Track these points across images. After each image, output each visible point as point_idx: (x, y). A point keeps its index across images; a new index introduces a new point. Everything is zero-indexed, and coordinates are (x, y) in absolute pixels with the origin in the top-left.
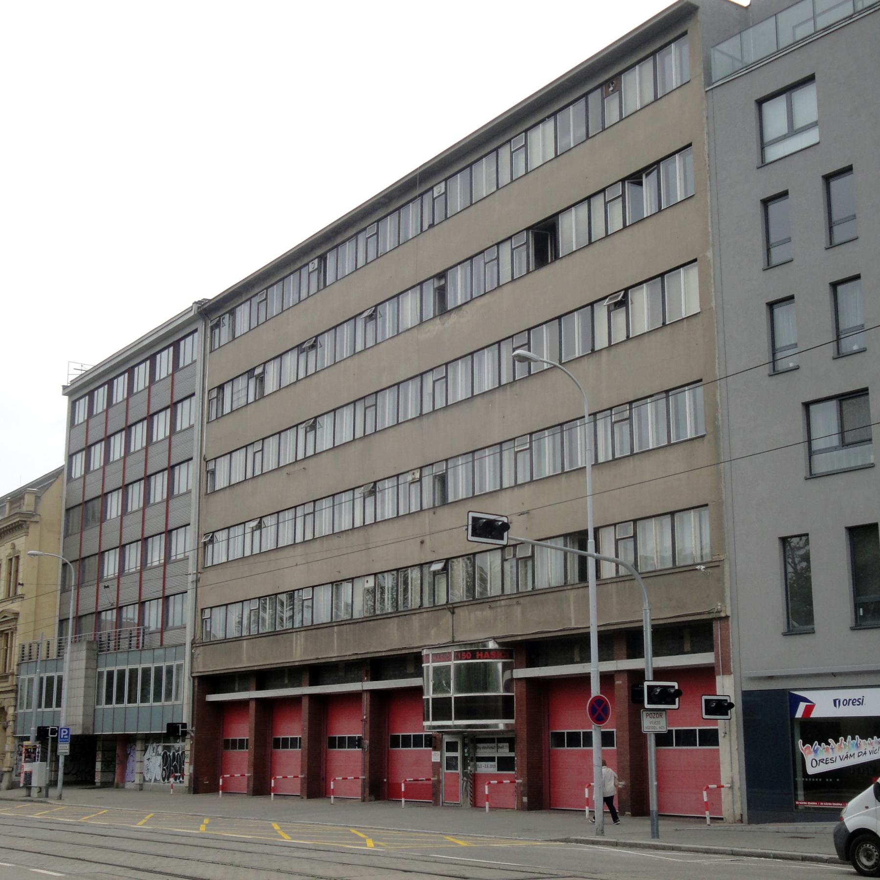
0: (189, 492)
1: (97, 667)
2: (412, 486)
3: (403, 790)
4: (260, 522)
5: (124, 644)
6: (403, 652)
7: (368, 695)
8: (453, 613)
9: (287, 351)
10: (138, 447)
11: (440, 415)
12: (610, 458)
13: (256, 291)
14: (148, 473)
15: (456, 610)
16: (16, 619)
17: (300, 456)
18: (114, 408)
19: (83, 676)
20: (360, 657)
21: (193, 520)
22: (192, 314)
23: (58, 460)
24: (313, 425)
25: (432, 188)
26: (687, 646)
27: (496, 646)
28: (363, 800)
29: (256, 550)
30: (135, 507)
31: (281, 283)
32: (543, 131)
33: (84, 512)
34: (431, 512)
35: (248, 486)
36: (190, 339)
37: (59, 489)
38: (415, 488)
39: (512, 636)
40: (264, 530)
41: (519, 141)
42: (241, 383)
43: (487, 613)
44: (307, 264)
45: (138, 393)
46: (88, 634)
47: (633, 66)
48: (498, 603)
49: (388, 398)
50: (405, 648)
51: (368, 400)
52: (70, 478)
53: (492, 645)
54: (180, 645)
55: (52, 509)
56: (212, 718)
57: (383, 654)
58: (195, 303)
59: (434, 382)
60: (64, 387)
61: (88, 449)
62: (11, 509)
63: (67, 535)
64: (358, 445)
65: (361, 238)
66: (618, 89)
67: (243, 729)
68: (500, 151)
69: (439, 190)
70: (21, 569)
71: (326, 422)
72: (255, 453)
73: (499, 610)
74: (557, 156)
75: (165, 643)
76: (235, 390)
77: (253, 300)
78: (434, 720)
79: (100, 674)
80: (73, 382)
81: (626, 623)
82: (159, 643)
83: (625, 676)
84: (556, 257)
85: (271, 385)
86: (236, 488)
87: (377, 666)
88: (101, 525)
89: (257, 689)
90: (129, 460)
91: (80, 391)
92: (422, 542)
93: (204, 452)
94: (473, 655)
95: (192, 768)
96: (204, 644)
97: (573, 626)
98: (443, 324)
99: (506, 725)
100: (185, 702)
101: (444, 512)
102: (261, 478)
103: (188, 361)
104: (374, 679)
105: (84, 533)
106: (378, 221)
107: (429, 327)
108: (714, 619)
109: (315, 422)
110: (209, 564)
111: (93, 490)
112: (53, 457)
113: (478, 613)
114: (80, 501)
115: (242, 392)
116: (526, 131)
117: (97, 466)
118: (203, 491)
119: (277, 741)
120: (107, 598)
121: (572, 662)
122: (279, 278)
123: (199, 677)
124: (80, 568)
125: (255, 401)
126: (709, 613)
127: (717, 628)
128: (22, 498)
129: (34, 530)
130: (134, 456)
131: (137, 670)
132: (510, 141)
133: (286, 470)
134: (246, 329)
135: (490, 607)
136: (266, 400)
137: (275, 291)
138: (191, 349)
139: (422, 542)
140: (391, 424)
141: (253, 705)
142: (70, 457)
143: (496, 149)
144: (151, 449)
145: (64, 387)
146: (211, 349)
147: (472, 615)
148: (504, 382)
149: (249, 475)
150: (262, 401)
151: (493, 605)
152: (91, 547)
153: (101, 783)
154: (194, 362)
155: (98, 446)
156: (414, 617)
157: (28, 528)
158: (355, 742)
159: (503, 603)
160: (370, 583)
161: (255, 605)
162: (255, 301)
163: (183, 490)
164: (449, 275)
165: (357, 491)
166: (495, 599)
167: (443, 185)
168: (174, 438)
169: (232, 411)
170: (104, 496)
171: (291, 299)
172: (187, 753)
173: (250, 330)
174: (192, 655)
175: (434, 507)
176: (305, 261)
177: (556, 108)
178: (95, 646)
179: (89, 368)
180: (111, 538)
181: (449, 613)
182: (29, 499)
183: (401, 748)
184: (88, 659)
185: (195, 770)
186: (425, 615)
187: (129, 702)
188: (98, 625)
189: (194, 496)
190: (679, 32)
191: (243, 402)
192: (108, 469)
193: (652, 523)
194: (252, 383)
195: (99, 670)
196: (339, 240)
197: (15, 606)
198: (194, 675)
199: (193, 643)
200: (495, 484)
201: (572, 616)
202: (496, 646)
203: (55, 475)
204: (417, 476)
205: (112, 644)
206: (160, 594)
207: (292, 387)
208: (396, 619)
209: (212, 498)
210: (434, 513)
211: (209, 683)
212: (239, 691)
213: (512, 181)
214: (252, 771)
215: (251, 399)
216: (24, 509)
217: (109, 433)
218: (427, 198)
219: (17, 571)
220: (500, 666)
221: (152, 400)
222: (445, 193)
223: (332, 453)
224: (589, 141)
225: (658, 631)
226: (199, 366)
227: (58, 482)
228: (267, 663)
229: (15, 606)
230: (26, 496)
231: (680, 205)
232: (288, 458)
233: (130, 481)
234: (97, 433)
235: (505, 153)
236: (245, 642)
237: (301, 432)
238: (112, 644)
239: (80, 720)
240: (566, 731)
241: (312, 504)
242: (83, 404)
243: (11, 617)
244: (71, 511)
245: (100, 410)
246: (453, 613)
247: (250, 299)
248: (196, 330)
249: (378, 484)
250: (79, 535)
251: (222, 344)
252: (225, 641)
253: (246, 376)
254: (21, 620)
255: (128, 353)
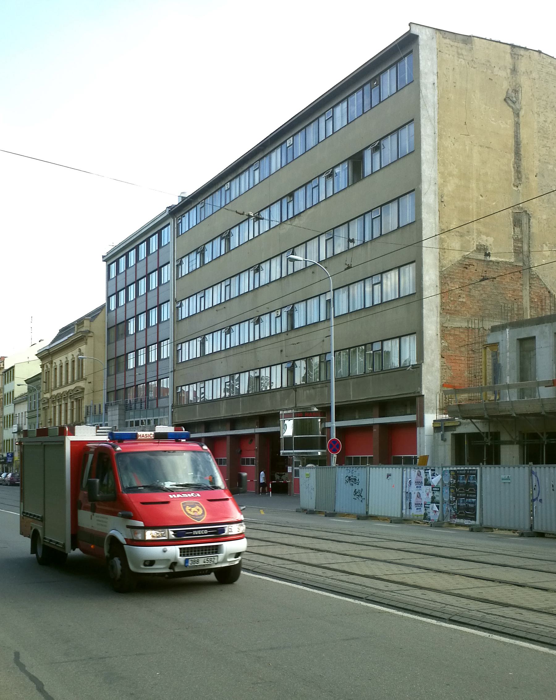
0: (168, 320)
2: (277, 319)
5: (138, 406)
6: (273, 412)
8: (296, 391)
11: (290, 277)
15: (297, 390)
16: (83, 392)
20: (252, 415)
22: (166, 214)
23: (103, 301)
24: (258, 269)
25: (286, 141)
26: (409, 411)
27: (317, 410)
31: (211, 196)
32: (342, 107)
33: (117, 330)
35: (198, 317)
37: (103, 316)
38: (278, 320)
39: (323, 404)
40: (261, 324)
41: (329, 114)
42: (217, 242)
43: (312, 391)
44: (224, 185)
46: (121, 401)
47: (386, 70)
50: (273, 410)
52: (109, 310)
54: (166, 407)
55: (99, 327)
57: (263, 413)
59: (326, 240)
60: (103, 257)
61: (117, 293)
62: (78, 329)
63: (109, 343)
64: (251, 294)
65: (252, 169)
66: (379, 84)
70: (84, 364)
72: (226, 286)
73: (317, 389)
74: (348, 123)
75: (159, 406)
76: (190, 260)
80: (108, 253)
81: (376, 398)
84: (364, 178)
86: (192, 318)
89: (205, 432)
90: (138, 300)
91: (111, 259)
92: (281, 351)
94: (303, 414)
97: (352, 399)
99: (322, 453)
101: (292, 334)
102: (203, 312)
105: (117, 342)
106: (259, 160)
107: (284, 226)
108: (416, 396)
109: (259, 267)
112: (98, 298)
113: (308, 391)
114: (115, 324)
118: (175, 320)
120: (130, 380)
122: (210, 194)
124: (117, 363)
125: (200, 267)
126: (414, 393)
127: (418, 399)
128: (83, 323)
129: (90, 341)
130: (141, 298)
132: (325, 113)
133: (216, 308)
134: (195, 224)
135: (313, 388)
136: (206, 266)
138: (167, 234)
139: (281, 351)
142: (108, 298)
144: (149, 294)
145: (103, 257)
146: (178, 234)
147: (305, 392)
149: (198, 311)
150: (229, 254)
151: (314, 386)
152: (121, 352)
154: (169, 243)
156: (277, 393)
157: (87, 340)
158: (253, 462)
159: (319, 386)
162: (199, 206)
163: (165, 319)
164: (296, 194)
165: (251, 321)
166: (316, 383)
167: (291, 139)
170: (126, 322)
172: (452, 432)
175: (288, 331)
176: (223, 183)
177: (347, 94)
178: (123, 407)
180: (130, 346)
182: (86, 323)
186: (283, 392)
189: (171, 321)
190: (409, 51)
191: (194, 268)
193: (407, 338)
194: (198, 256)
195: (126, 420)
196: (240, 171)
197: (81, 384)
200: (361, 305)
201: (351, 393)
202: (317, 410)
203: (101, 308)
204: (279, 313)
206: (144, 381)
209: (180, 324)
212: (197, 433)
213: (326, 138)
215: (198, 266)
216: (83, 329)
217: (127, 284)
218: (284, 147)
219: (82, 364)
222: (293, 144)
223: (237, 299)
226: (171, 245)
227: (103, 312)
229: (81, 384)
230: (85, 321)
231: (408, 157)
232: (275, 275)
234: (121, 285)
237: (252, 273)
241: (380, 275)
242: (113, 266)
243: (80, 390)
244: (110, 330)
246: (296, 391)
247: (196, 206)
248: (169, 224)
249: (296, 306)
250: (114, 344)
252: (213, 401)
254: (86, 392)
255: (135, 237)
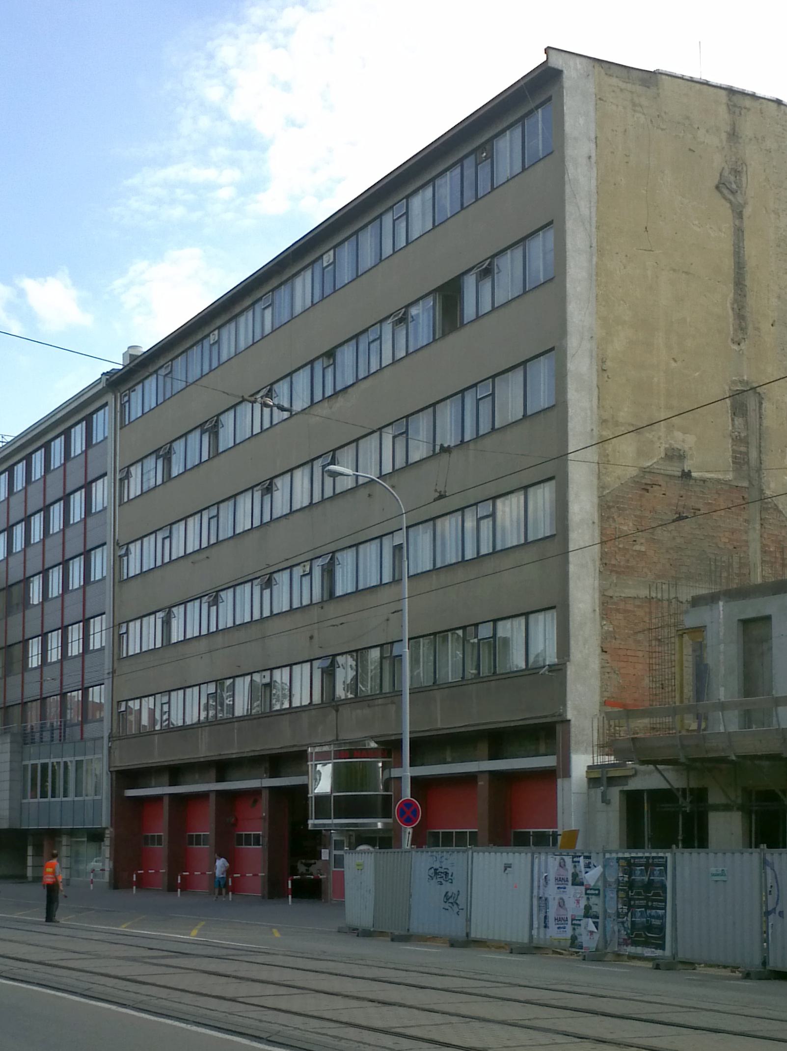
1: (22, 760)
2: (304, 579)
3: (290, 887)
4: (332, 559)
5: (47, 736)
7: (267, 791)
8: (337, 711)
9: (299, 369)
10: (77, 519)
12: (522, 541)
13: (162, 362)
14: (66, 558)
15: (340, 709)
17: (205, 544)
18: (94, 449)
19: (8, 769)
21: (109, 609)
22: (100, 387)
24: (269, 489)
28: (263, 897)
29: (213, 629)
30: (55, 594)
34: (320, 605)
36: (101, 413)
44: (208, 335)
45: (75, 457)
47: (503, 131)
48: (376, 702)
49: (422, 423)
51: (402, 426)
53: (373, 745)
56: (131, 814)
58: (103, 374)
64: (256, 535)
65: (258, 308)
67: (160, 828)
68: (384, 217)
69: (328, 258)
71: (282, 484)
74: (434, 227)
75: (85, 736)
77: (159, 372)
78: (316, 819)
79: (25, 767)
82: (79, 737)
83: (487, 775)
84: (463, 325)
85: (226, 439)
87: (498, 741)
88: (24, 611)
92: (311, 638)
93: (117, 538)
94: (351, 754)
95: (112, 863)
96: (120, 739)
97: (439, 726)
98: (331, 408)
99: (385, 824)
100: (104, 796)
103: (100, 438)
104: (272, 776)
105: (9, 619)
110: (125, 655)
111: (16, 575)
113: (359, 711)
115: (195, 447)
116: (407, 197)
117: (56, 529)
118: (117, 580)
119: (146, 837)
120: (33, 691)
121: (537, 755)
123: (117, 771)
125: (209, 459)
127: (559, 728)
131: (47, 764)
136: (173, 482)
137: (179, 363)
138: (103, 422)
139: (311, 638)
140: (486, 432)
141: (213, 798)
143: (380, 216)
146: (122, 423)
148: (467, 438)
149: (159, 563)
153: (33, 877)
154: (105, 438)
155: (57, 506)
159: (380, 702)
160: (212, 688)
161: (212, 688)
163: (98, 577)
168: (89, 521)
169: (494, 309)
171: (368, 259)
173: (157, 405)
174: (110, 748)
177: (434, 173)
179: (9, 439)
181: (334, 712)
183: (194, 846)
184: (12, 752)
185: (115, 863)
186: (313, 712)
187: (53, 797)
188: (24, 718)
189: (109, 583)
190: (543, 98)
191: (152, 484)
192: (48, 541)
193: (541, 616)
196: (238, 309)
198: (112, 769)
199: (110, 737)
204: (308, 569)
205: (37, 735)
207: (196, 469)
208: (288, 716)
210: (322, 608)
211: (126, 777)
214: (267, 871)
217: (28, 513)
218: (317, 268)
220: (380, 765)
221: (48, 490)
222: (334, 262)
223: (231, 542)
224: (463, 211)
225: (415, 743)
226: (110, 443)
228: (267, 747)
233: (50, 565)
235: (388, 220)
236: (156, 736)
237: (258, 495)
238: (37, 735)
239: (6, 813)
240: (441, 831)
245: (57, 464)
246: (337, 711)
248: (106, 404)
251: (132, 420)
252: (184, 728)
253: (154, 456)
255: (43, 427)
